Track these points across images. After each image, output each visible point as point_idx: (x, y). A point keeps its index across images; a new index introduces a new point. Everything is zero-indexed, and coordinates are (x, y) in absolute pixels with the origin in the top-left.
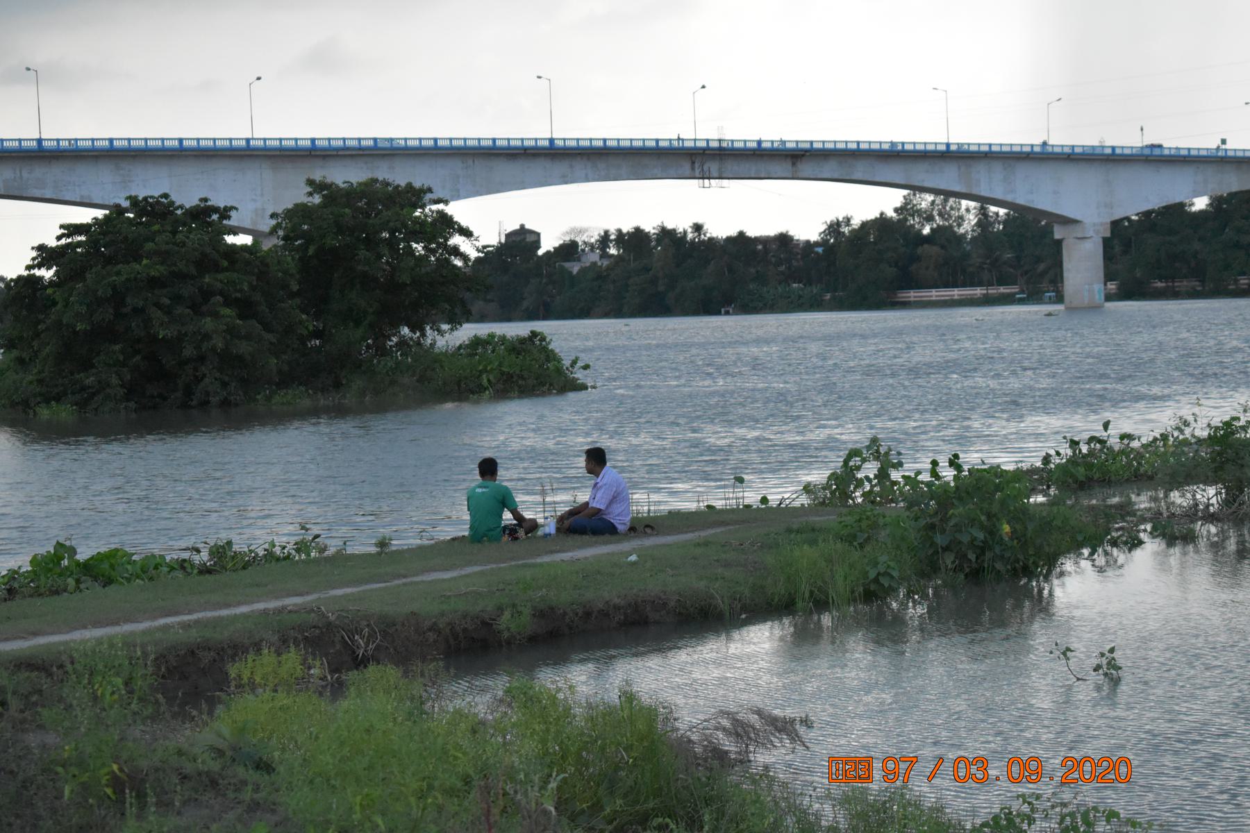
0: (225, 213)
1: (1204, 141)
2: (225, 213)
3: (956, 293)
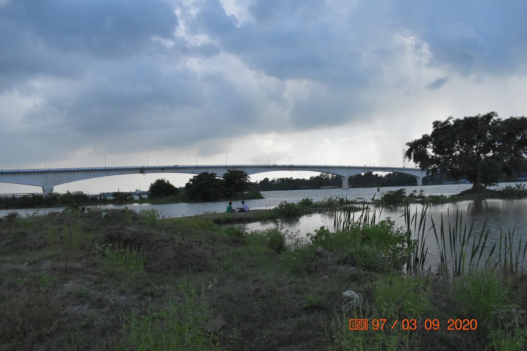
0: (215, 174)
1: (362, 165)
2: (215, 174)
3: (328, 187)
